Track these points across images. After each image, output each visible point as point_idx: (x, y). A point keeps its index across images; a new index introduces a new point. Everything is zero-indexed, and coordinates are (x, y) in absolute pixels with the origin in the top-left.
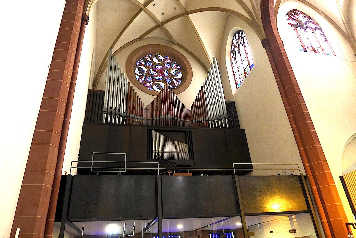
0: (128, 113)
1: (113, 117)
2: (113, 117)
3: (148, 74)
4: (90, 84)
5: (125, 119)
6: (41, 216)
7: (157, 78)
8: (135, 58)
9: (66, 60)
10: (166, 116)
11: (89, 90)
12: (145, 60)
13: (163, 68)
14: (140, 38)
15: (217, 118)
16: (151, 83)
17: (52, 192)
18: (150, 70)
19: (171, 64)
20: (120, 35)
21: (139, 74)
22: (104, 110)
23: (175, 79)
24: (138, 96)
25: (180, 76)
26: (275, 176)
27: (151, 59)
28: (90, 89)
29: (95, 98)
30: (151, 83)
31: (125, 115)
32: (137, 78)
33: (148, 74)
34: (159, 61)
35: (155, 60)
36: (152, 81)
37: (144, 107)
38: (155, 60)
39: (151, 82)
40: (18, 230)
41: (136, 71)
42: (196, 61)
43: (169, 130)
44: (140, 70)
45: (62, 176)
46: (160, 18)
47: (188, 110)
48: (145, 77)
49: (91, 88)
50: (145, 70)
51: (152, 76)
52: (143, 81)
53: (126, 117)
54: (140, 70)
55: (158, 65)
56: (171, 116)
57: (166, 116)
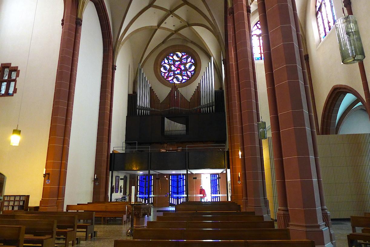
0: (151, 108)
1: (143, 111)
2: (143, 111)
3: (170, 70)
4: (130, 85)
5: (149, 111)
6: (104, 171)
7: (176, 72)
8: (160, 59)
9: (106, 100)
10: (173, 107)
11: (128, 94)
12: (168, 59)
13: (181, 64)
14: (163, 42)
15: (208, 106)
16: (172, 77)
17: (107, 160)
18: (172, 66)
19: (187, 58)
20: (146, 48)
21: (164, 71)
22: (137, 108)
23: (189, 71)
24: (156, 96)
25: (193, 68)
26: (44, 179)
27: (172, 57)
28: (130, 94)
29: (132, 99)
30: (172, 77)
31: (149, 109)
32: (163, 74)
33: (170, 70)
34: (166, 71)
35: (175, 58)
36: (173, 76)
37: (160, 103)
38: (175, 58)
39: (172, 76)
40: (96, 175)
41: (162, 69)
42: (205, 54)
43: (174, 117)
44: (165, 68)
45: (111, 153)
46: (173, 29)
47: (188, 101)
48: (168, 73)
49: (131, 93)
50: (168, 67)
51: (174, 71)
52: (166, 76)
53: (150, 110)
54: (165, 68)
55: (177, 61)
56: (176, 108)
57: (173, 107)
